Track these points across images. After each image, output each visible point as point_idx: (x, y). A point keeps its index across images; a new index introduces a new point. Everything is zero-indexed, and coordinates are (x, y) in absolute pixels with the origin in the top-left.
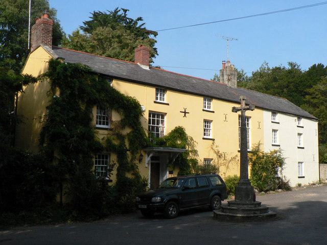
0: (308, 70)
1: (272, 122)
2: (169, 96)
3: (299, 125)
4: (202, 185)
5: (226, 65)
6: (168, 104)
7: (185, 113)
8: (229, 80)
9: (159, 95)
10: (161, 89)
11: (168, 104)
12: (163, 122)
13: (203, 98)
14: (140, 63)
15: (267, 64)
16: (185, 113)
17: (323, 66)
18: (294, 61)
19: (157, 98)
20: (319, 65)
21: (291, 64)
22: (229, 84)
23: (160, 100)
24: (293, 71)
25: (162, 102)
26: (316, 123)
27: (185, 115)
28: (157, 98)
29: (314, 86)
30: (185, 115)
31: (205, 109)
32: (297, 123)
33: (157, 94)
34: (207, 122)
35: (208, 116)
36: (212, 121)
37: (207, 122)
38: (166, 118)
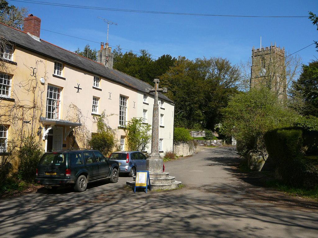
0: (157, 59)
1: (93, 88)
2: (66, 72)
3: (145, 102)
4: (62, 127)
5: (105, 47)
6: (64, 79)
7: (78, 88)
8: (107, 61)
9: (96, 82)
10: (60, 64)
11: (64, 79)
12: (59, 96)
13: (53, 64)
14: (31, 33)
15: (89, 46)
16: (78, 88)
17: (171, 57)
18: (143, 49)
19: (55, 72)
20: (168, 56)
21: (143, 52)
22: (107, 66)
23: (58, 74)
24: (144, 59)
25: (59, 75)
26: (173, 107)
27: (78, 90)
28: (55, 72)
29: (163, 74)
30: (78, 90)
31: (94, 86)
32: (143, 100)
33: (55, 69)
34: (96, 99)
35: (97, 94)
36: (99, 98)
37: (96, 99)
38: (61, 93)
